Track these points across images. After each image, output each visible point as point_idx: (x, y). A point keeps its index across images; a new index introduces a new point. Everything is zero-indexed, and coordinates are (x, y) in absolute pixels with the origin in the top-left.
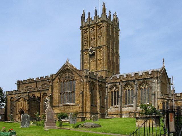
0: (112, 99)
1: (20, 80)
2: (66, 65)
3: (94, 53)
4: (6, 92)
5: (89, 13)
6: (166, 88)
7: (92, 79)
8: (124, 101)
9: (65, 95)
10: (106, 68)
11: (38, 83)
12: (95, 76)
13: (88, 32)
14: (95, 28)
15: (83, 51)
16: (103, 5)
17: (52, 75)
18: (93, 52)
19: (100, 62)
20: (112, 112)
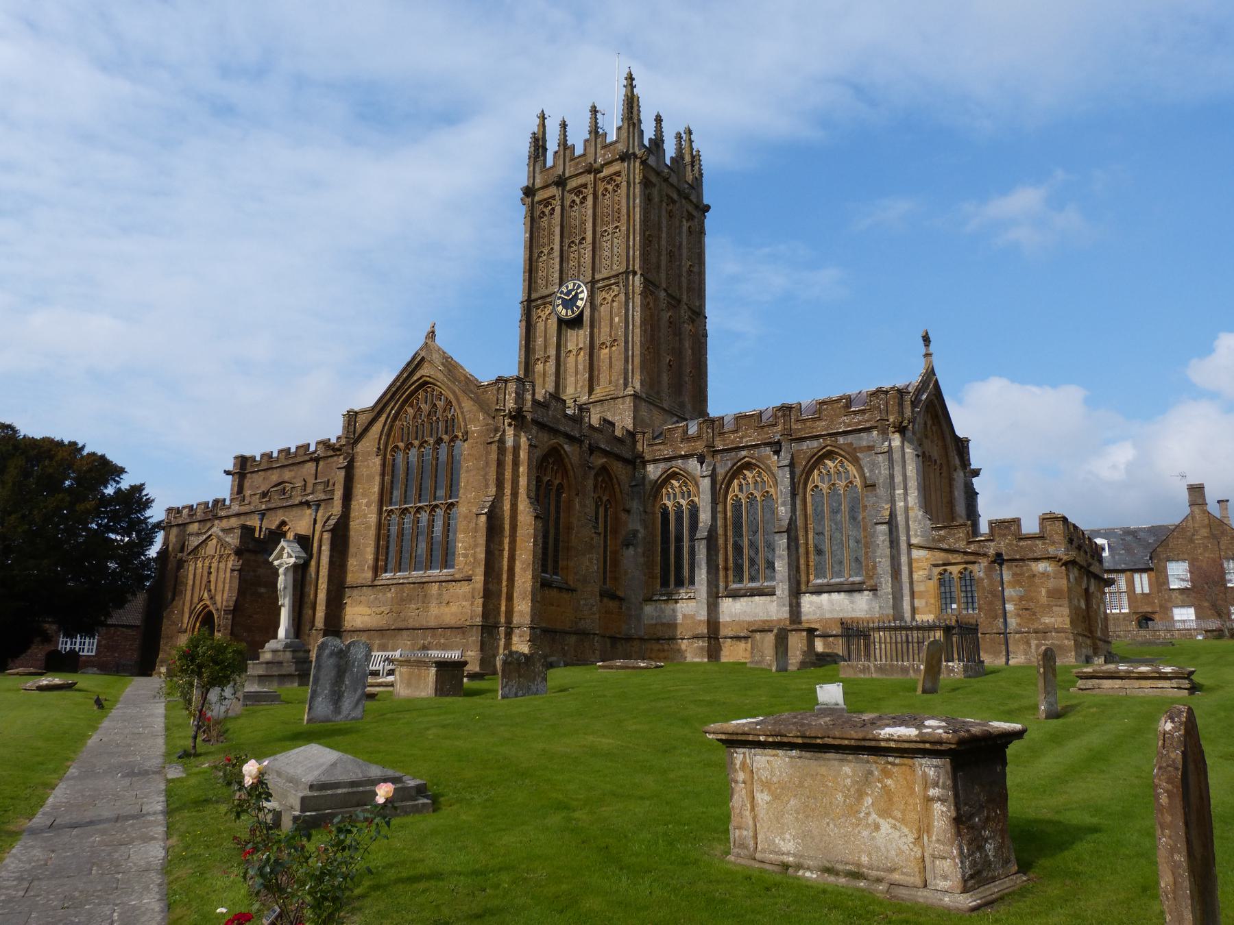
0: (665, 551)
1: (247, 453)
3: (582, 313)
5: (564, 125)
6: (951, 492)
10: (638, 386)
12: (572, 418)
13: (558, 209)
16: (625, 82)
18: (578, 307)
19: (610, 358)
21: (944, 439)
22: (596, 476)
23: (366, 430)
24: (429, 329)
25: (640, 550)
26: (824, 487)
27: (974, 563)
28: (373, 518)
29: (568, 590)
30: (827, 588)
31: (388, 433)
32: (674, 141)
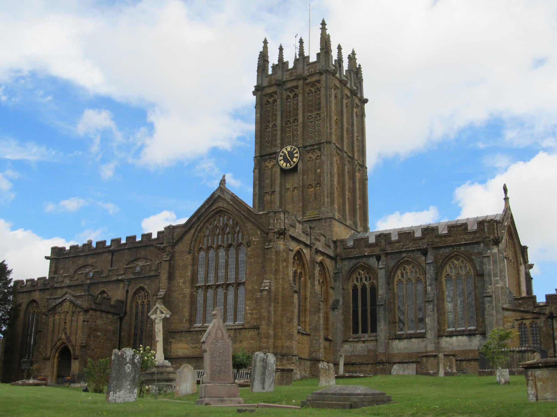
2: (219, 196)
3: (296, 166)
5: (281, 49)
11: (116, 254)
13: (279, 101)
14: (299, 91)
16: (321, 26)
18: (294, 162)
19: (315, 194)
20: (355, 356)
21: (515, 248)
23: (181, 238)
24: (221, 178)
25: (341, 311)
27: (538, 318)
29: (306, 334)
30: (455, 333)
32: (337, 50)
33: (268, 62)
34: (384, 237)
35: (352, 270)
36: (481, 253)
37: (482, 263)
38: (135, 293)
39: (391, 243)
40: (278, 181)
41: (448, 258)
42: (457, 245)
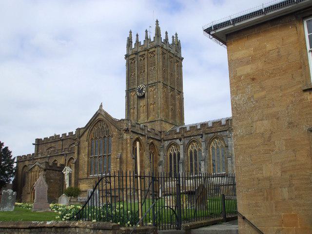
0: (171, 166)
1: (39, 138)
4: (18, 157)
7: (138, 134)
8: (188, 169)
9: (97, 160)
12: (141, 129)
14: (145, 56)
15: (128, 92)
17: (78, 130)
22: (150, 145)
26: (215, 147)
28: (86, 159)
31: (89, 135)
33: (132, 42)
34: (193, 127)
35: (170, 146)
36: (227, 136)
37: (228, 141)
38: (69, 161)
39: (186, 132)
40: (136, 103)
41: (212, 139)
42: (216, 132)
